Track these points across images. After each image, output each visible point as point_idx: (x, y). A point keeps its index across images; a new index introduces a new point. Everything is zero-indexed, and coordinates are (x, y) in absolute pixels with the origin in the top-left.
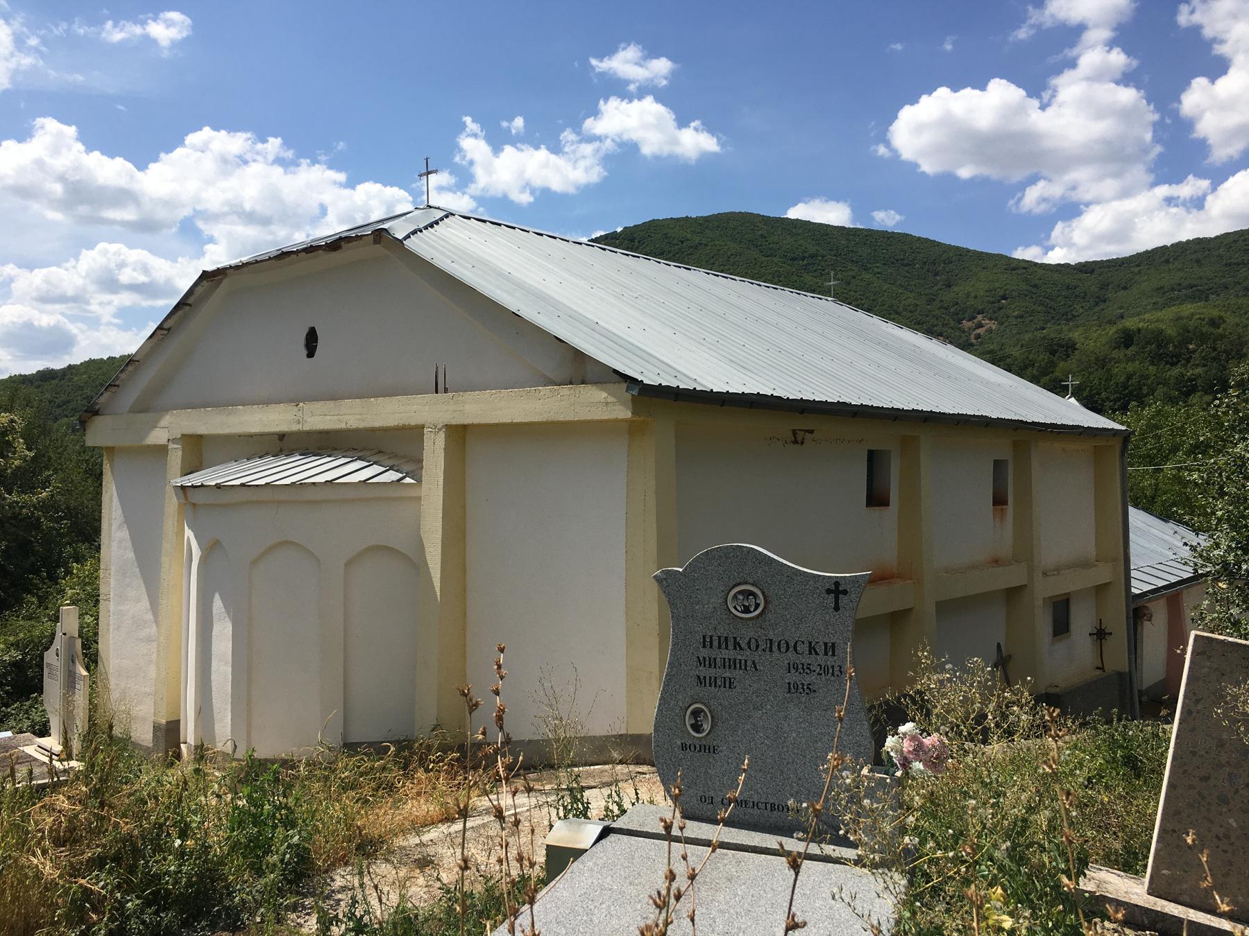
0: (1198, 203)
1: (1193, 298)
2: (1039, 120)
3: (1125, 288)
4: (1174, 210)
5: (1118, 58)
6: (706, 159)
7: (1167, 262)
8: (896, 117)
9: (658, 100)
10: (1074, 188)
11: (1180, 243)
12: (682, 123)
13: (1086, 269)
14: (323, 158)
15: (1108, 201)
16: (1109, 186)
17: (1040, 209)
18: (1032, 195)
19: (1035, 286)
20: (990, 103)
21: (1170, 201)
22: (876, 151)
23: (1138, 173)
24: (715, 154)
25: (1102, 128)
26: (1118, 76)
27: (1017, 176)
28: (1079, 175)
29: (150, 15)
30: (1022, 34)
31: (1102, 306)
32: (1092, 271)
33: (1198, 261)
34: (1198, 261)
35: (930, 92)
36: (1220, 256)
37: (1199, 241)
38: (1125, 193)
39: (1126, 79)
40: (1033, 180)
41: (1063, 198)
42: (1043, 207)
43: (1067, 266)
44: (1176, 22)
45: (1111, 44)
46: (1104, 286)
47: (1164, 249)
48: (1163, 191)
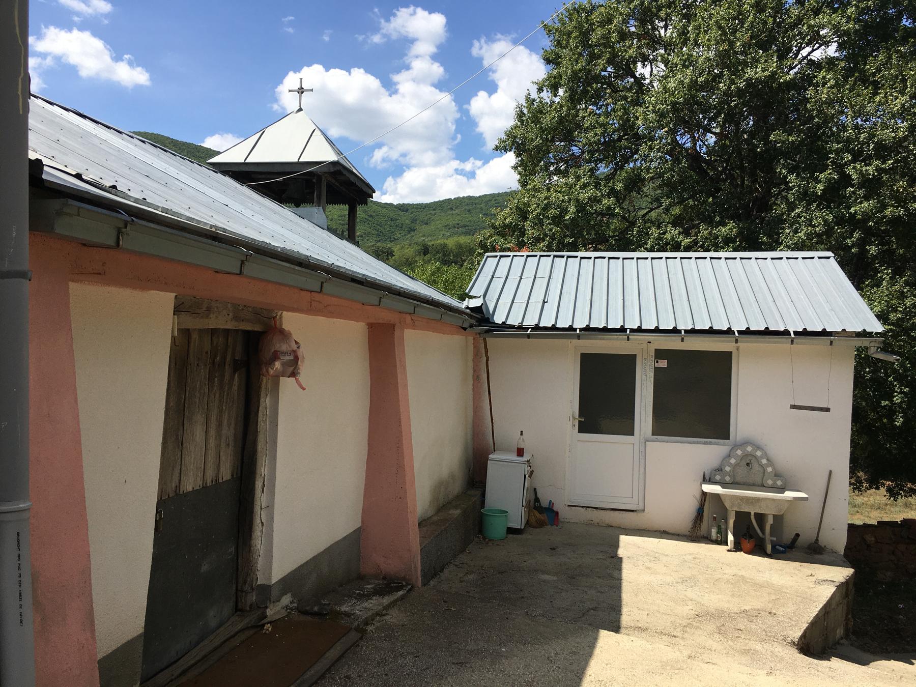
0: (472, 175)
1: (466, 234)
2: (388, 104)
3: (427, 224)
4: (459, 177)
5: (437, 70)
6: (138, 88)
7: (452, 209)
8: (282, 83)
9: (96, 33)
10: (404, 155)
11: (459, 198)
12: (117, 58)
13: (403, 208)
14: (276, 107)
15: (425, 166)
16: (429, 157)
17: (382, 166)
18: (378, 155)
19: (371, 216)
20: (353, 85)
21: (458, 171)
22: (272, 108)
23: (444, 151)
24: (147, 87)
25: (427, 115)
26: (436, 82)
27: (369, 142)
28: (406, 145)
29: (379, 167)
30: (377, 39)
31: (413, 233)
32: (407, 210)
33: (469, 211)
34: (469, 211)
35: (309, 65)
36: (481, 208)
37: (470, 198)
38: (437, 163)
39: (440, 86)
40: (379, 146)
41: (397, 160)
42: (385, 165)
43: (391, 205)
44: (471, 54)
45: (435, 58)
46: (414, 221)
47: (449, 201)
48: (455, 164)
